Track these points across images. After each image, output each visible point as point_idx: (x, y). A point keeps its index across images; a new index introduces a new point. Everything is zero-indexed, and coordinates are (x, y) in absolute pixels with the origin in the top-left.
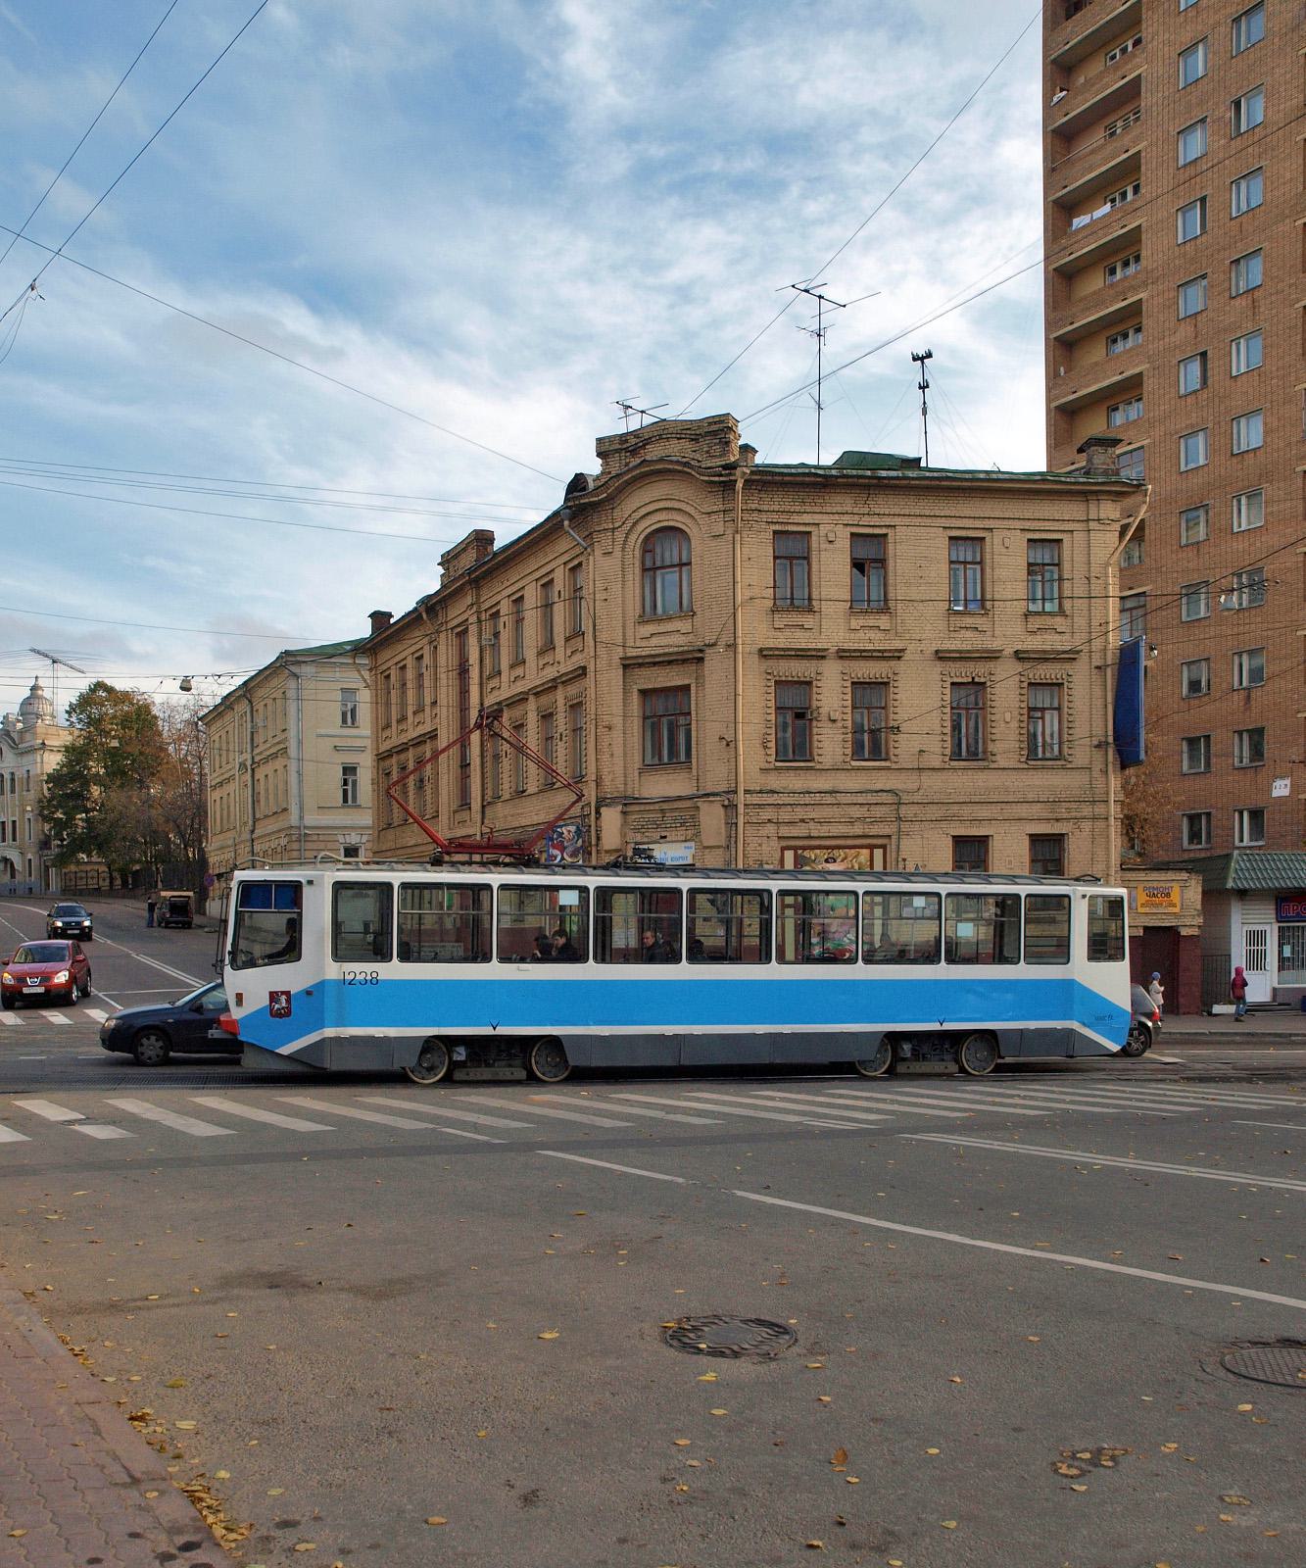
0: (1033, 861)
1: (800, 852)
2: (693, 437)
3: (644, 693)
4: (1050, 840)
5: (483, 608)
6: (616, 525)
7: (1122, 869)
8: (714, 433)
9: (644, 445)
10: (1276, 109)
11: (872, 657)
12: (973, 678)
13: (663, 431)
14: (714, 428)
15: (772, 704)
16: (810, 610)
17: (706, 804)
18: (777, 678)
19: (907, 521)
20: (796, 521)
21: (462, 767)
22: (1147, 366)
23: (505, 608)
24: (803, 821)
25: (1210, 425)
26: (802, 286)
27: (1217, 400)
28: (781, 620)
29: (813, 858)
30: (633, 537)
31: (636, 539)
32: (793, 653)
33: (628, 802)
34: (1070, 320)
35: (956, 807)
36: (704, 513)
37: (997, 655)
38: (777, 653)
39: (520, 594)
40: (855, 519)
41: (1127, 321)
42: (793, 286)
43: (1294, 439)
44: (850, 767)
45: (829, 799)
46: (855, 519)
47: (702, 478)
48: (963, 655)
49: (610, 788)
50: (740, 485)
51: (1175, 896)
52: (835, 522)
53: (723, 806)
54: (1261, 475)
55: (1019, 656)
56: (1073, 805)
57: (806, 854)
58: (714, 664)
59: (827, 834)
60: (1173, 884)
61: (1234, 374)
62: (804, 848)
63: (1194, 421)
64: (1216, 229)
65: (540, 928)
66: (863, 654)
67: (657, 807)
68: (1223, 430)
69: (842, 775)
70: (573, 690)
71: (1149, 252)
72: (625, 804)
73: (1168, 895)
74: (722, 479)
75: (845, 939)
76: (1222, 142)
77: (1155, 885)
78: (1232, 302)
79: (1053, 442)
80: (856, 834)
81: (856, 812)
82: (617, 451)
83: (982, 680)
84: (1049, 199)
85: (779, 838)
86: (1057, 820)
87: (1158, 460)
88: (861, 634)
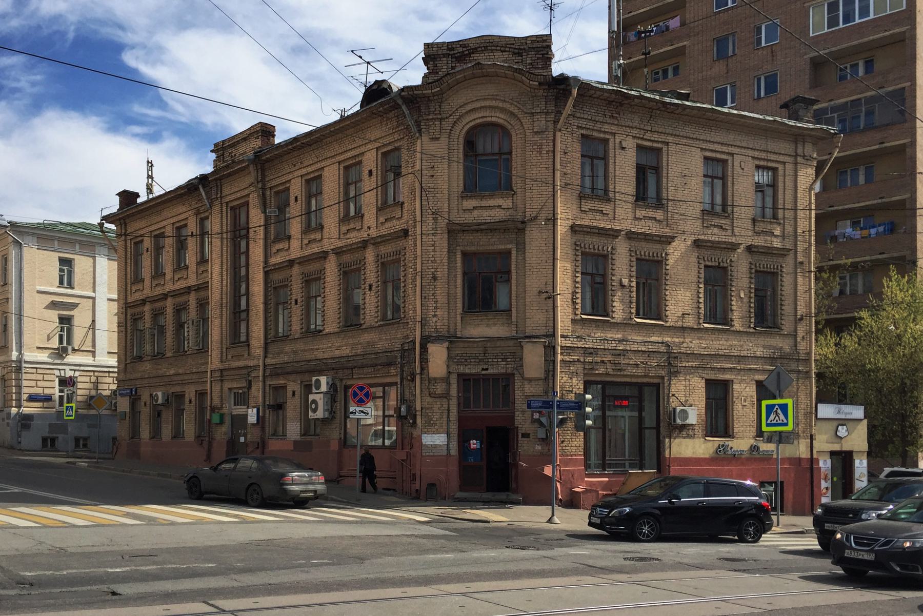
6: (444, 116)
9: (470, 54)
12: (719, 263)
16: (609, 200)
17: (530, 344)
18: (583, 250)
19: (677, 140)
23: (297, 188)
28: (586, 205)
33: (451, 339)
52: (627, 134)
55: (749, 249)
58: (535, 237)
82: (444, 55)
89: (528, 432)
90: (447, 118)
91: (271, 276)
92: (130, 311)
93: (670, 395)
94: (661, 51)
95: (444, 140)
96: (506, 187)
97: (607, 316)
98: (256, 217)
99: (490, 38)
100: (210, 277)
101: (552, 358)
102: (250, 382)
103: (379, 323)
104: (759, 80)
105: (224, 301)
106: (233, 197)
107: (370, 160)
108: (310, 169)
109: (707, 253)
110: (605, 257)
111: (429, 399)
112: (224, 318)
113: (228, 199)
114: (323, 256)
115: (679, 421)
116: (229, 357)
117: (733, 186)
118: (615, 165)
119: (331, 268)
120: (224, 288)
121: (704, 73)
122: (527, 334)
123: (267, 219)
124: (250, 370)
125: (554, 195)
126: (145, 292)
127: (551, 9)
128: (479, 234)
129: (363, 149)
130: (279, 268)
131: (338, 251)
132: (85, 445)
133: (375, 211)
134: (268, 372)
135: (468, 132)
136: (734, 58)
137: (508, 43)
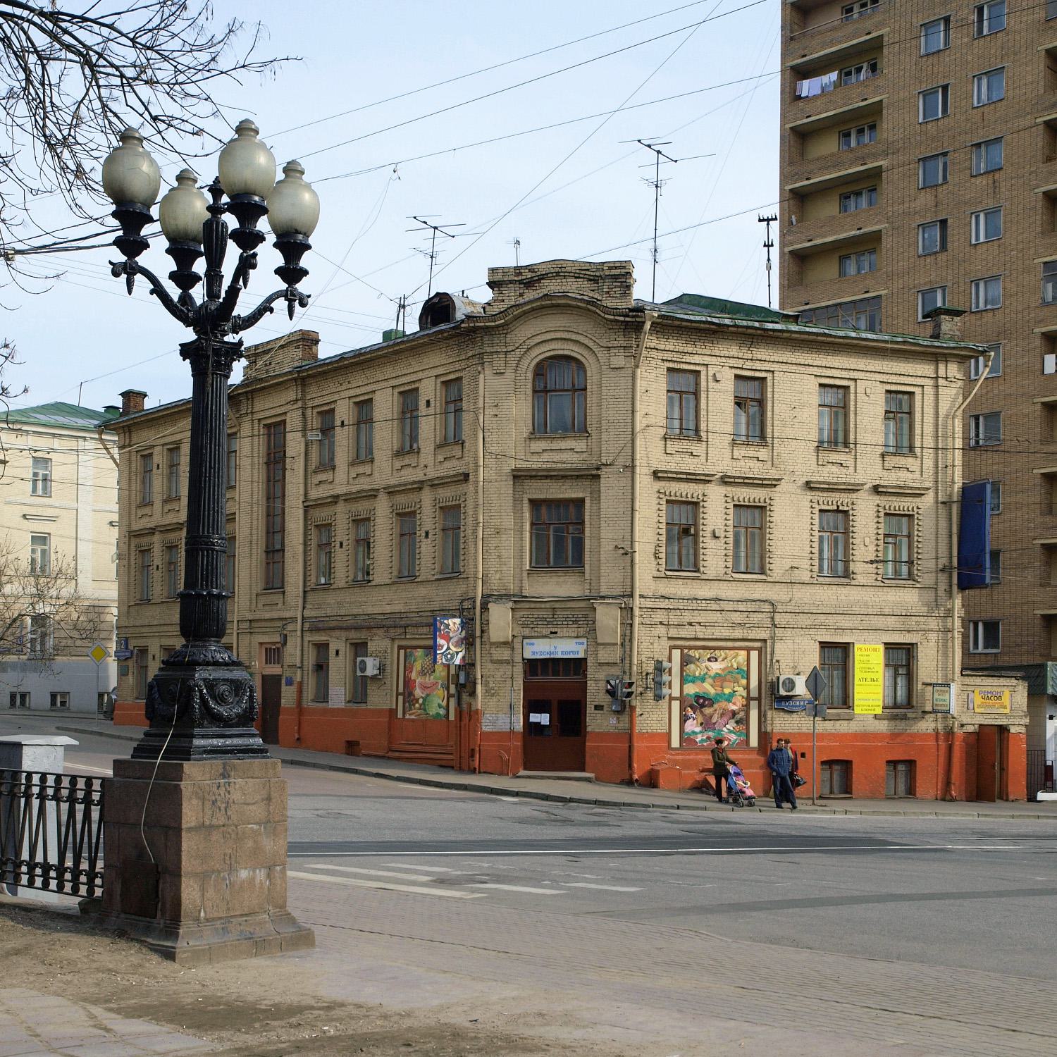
0: (887, 665)
1: (686, 651)
2: (592, 278)
3: (533, 502)
4: (836, 647)
5: (310, 404)
6: (510, 348)
7: (962, 675)
8: (615, 277)
9: (540, 279)
10: (1018, 19)
11: (763, 484)
12: (838, 507)
13: (559, 270)
14: (614, 272)
15: (663, 520)
19: (784, 367)
20: (688, 361)
21: (267, 552)
22: (887, 225)
23: (344, 412)
24: (690, 624)
25: (950, 284)
26: (647, 143)
27: (956, 263)
28: (673, 446)
29: (697, 657)
30: (525, 363)
31: (529, 364)
32: (685, 476)
33: (518, 600)
34: (806, 175)
35: (822, 617)
36: (602, 347)
37: (858, 488)
38: (670, 475)
39: (370, 397)
40: (740, 363)
41: (868, 182)
42: (639, 141)
43: (1032, 305)
44: (731, 579)
45: (714, 606)
46: (740, 363)
47: (606, 316)
48: (831, 487)
49: (495, 586)
50: (648, 325)
51: (1006, 699)
53: (621, 608)
54: (999, 333)
55: (876, 490)
56: (922, 619)
57: (692, 653)
58: (610, 483)
59: (710, 637)
60: (1004, 689)
61: (973, 242)
62: (690, 648)
63: (933, 278)
64: (958, 115)
65: (391, 710)
66: (746, 481)
67: (548, 605)
68: (961, 289)
69: (723, 585)
70: (446, 494)
71: (890, 126)
72: (515, 601)
73: (1000, 698)
74: (627, 319)
75: (724, 729)
76: (965, 40)
77: (989, 689)
78: (973, 180)
79: (786, 282)
80: (736, 637)
81: (737, 618)
83: (846, 509)
84: (788, 64)
85: (669, 638)
86: (909, 631)
87: (895, 309)
88: (742, 463)
89: (602, 704)
90: (513, 351)
91: (311, 512)
92: (134, 541)
93: (774, 661)
94: (850, 171)
95: (510, 373)
96: (580, 429)
97: (698, 571)
98: (294, 444)
99: (562, 262)
100: (237, 507)
101: (629, 622)
102: (286, 636)
103: (436, 577)
104: (977, 218)
105: (255, 538)
106: (267, 414)
107: (429, 390)
108: (359, 391)
109: (822, 496)
110: (696, 504)
111: (490, 666)
112: (254, 557)
113: (262, 415)
114: (372, 495)
115: (783, 692)
116: (260, 606)
117: (856, 416)
118: (708, 401)
119: (382, 509)
120: (255, 523)
121: (907, 205)
122: (602, 594)
123: (308, 445)
124: (284, 622)
125: (633, 440)
126: (154, 518)
127: (657, 187)
128: (549, 481)
129: (420, 376)
130: (321, 504)
131: (390, 490)
132: (63, 703)
133: (432, 448)
134: (307, 626)
135: (538, 364)
136: (945, 187)
137: (583, 268)
